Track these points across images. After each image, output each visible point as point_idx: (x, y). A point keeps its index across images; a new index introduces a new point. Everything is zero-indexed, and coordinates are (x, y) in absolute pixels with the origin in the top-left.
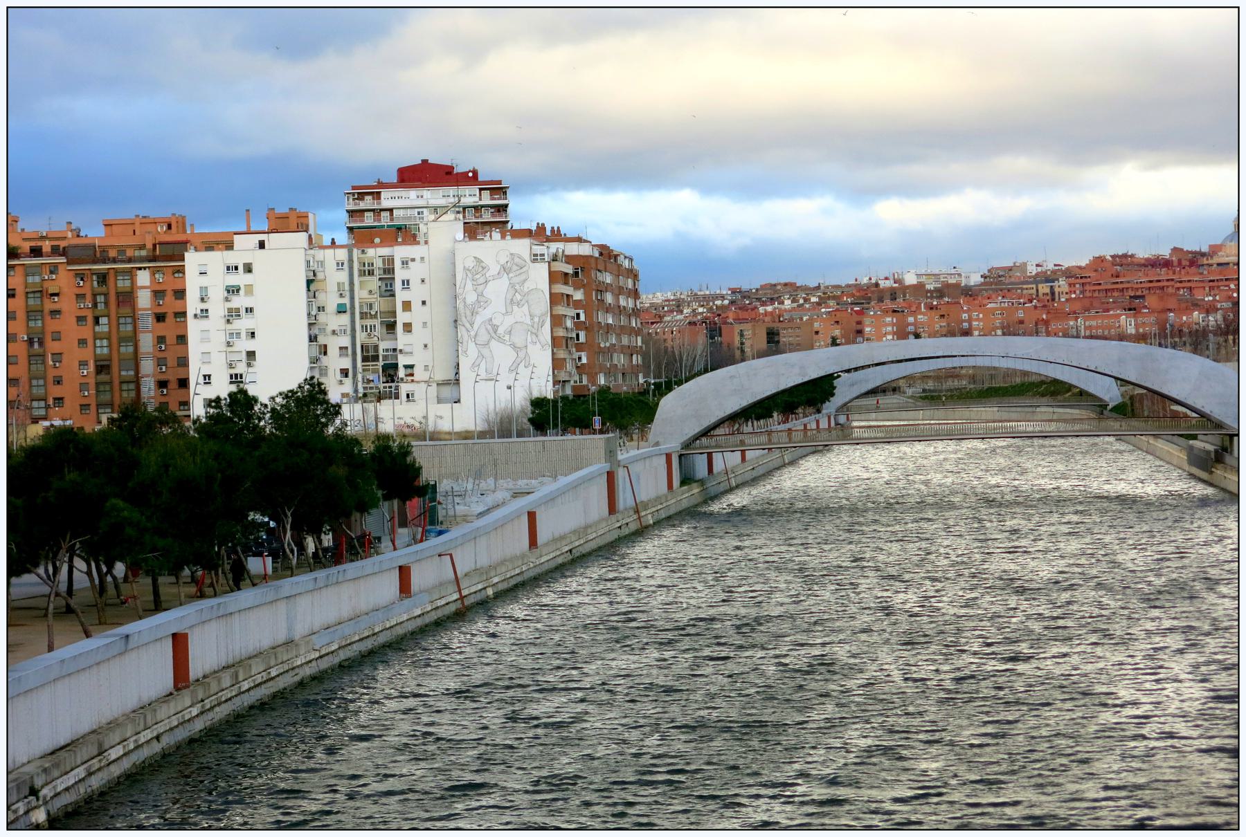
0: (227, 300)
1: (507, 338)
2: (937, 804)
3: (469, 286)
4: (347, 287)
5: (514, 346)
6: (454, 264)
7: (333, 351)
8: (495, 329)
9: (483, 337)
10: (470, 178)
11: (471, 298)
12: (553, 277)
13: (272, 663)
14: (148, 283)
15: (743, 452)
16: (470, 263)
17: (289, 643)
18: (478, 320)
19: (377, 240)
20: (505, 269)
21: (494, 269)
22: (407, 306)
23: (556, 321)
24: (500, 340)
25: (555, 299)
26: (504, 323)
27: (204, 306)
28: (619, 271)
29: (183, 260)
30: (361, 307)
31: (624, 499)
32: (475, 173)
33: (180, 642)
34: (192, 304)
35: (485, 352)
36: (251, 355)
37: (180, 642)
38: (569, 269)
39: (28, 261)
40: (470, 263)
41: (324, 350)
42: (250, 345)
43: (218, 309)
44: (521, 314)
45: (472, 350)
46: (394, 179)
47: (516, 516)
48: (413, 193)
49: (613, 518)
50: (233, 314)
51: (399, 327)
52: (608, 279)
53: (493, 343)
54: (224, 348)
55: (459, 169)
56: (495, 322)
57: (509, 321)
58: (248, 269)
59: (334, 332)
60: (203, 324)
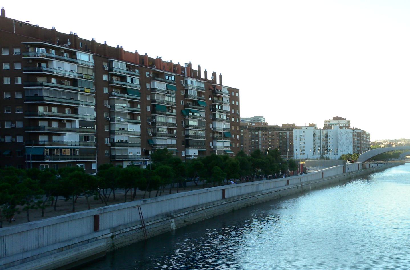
0: (300, 137)
1: (345, 145)
2: (218, 204)
3: (340, 136)
4: (320, 136)
5: (347, 146)
6: (337, 133)
7: (317, 146)
8: (344, 143)
9: (342, 145)
10: (344, 119)
11: (340, 138)
12: (353, 135)
13: (250, 195)
14: (289, 134)
15: (378, 164)
16: (340, 133)
17: (256, 192)
18: (341, 142)
19: (326, 128)
20: (345, 134)
21: (344, 134)
22: (330, 139)
23: (354, 142)
24: (344, 145)
25: (354, 139)
26: (345, 143)
27: (296, 138)
28: (366, 135)
29: (293, 130)
30: (322, 139)
31: (347, 171)
32: (345, 118)
33: (224, 191)
34: (294, 138)
35: (342, 147)
36: (304, 146)
37: (224, 191)
38: (356, 134)
39: (269, 130)
40: (340, 133)
41: (316, 146)
42: (304, 145)
43: (298, 139)
44: (348, 141)
45: (340, 147)
46: (332, 119)
47: (319, 172)
48: (335, 121)
49: (344, 174)
50: (300, 140)
51: (328, 142)
52: (365, 136)
53: (343, 146)
54: (299, 145)
55: (343, 118)
56: (344, 142)
57: (346, 142)
58: (304, 132)
59: (318, 143)
60: (296, 141)
